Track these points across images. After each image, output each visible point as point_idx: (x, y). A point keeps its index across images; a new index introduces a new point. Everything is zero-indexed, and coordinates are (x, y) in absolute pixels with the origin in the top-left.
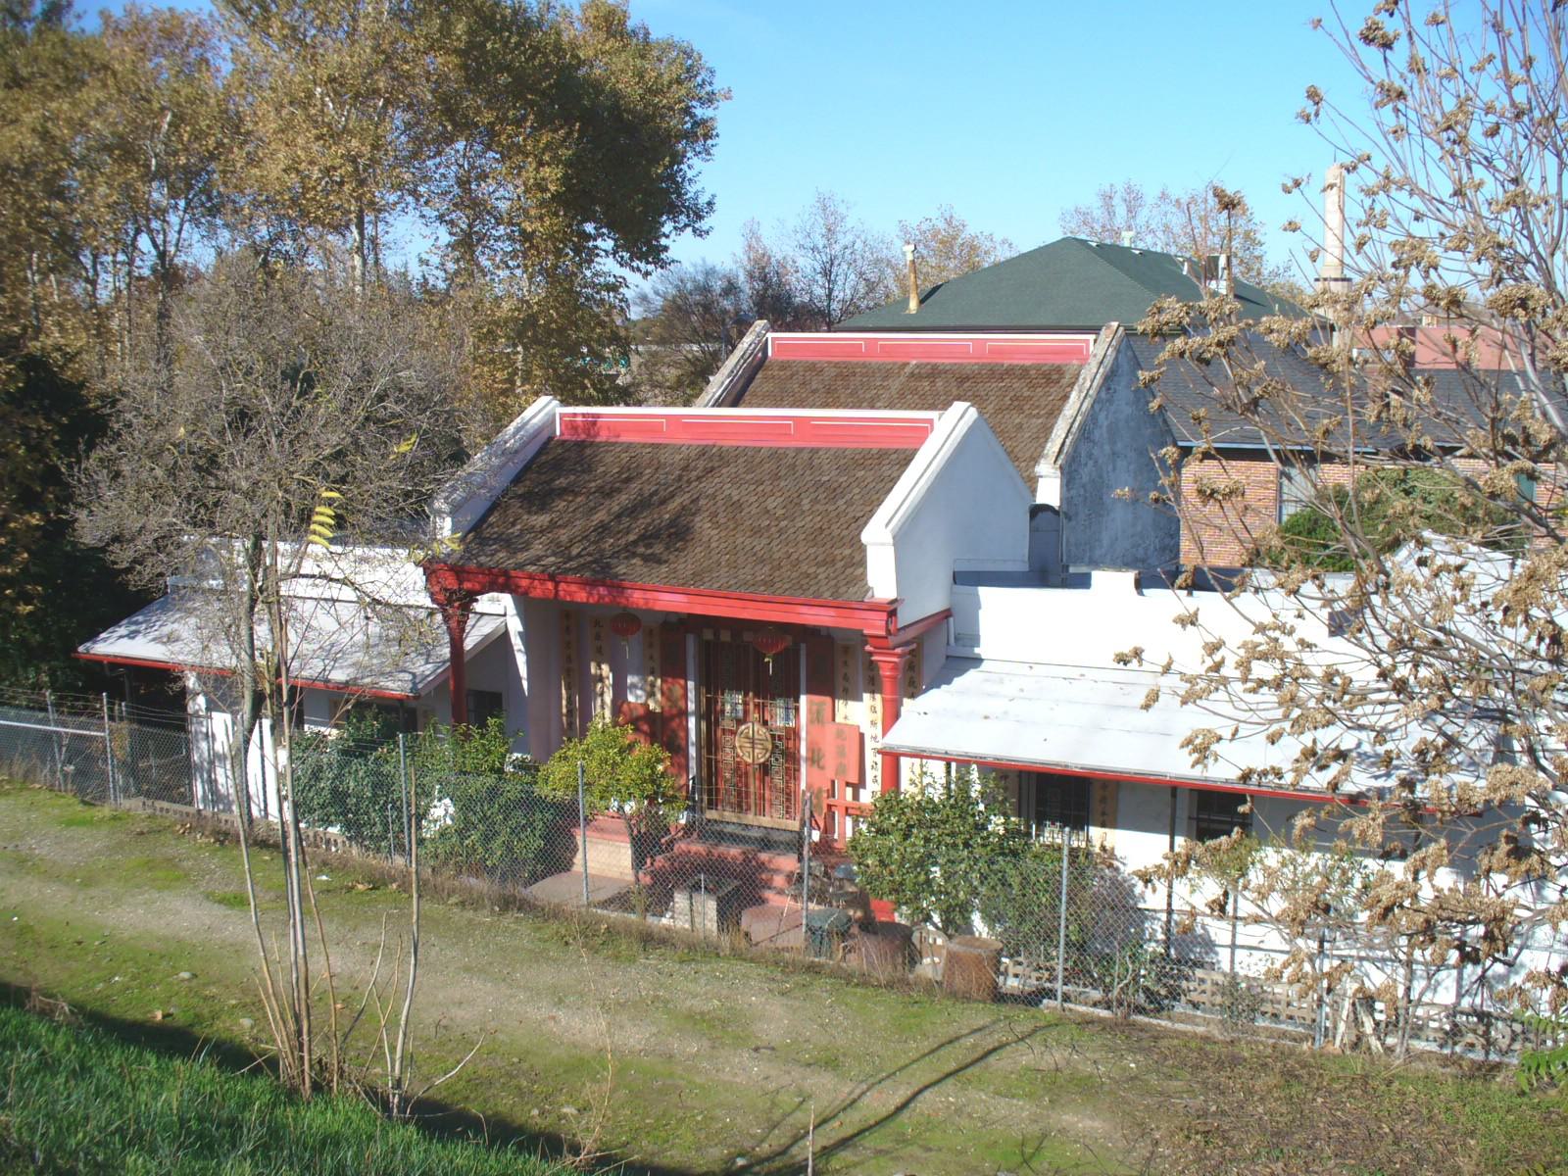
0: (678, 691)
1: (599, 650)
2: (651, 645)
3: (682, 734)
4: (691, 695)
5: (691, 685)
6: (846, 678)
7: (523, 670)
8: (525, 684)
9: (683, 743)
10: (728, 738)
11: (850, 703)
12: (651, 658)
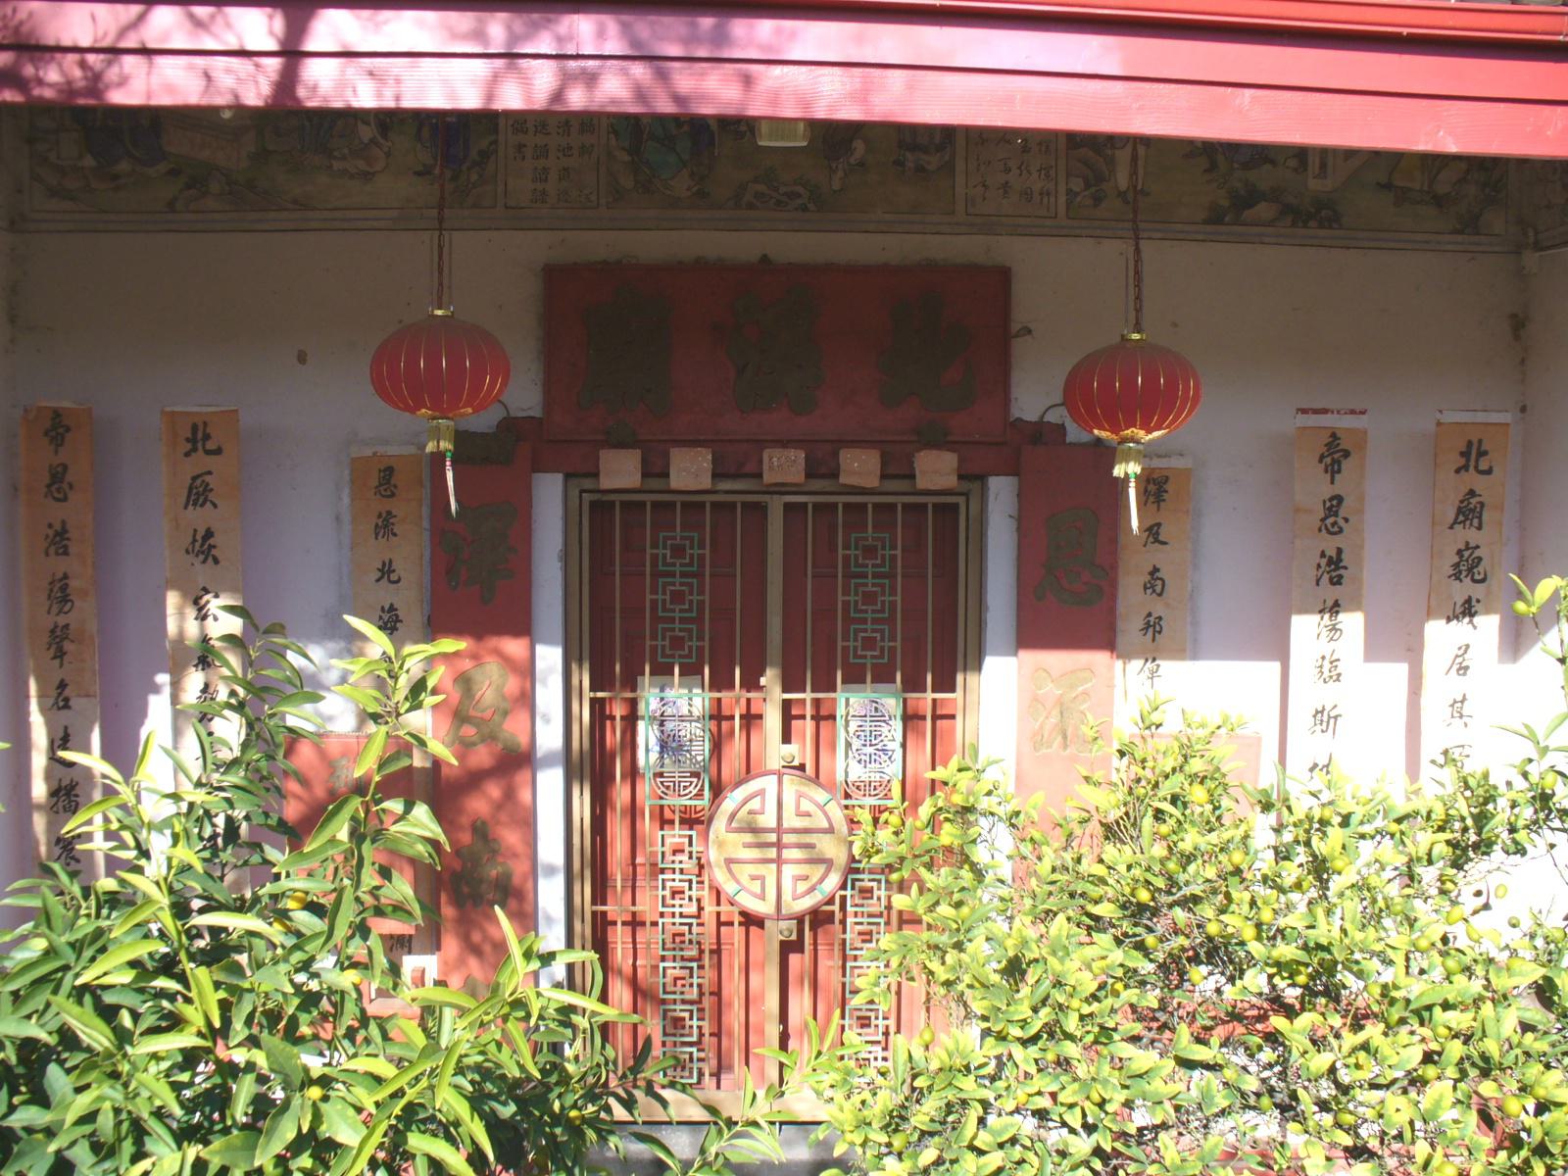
0: (492, 682)
1: (204, 547)
2: (385, 526)
3: (511, 837)
4: (549, 695)
5: (549, 658)
6: (1154, 582)
7: (450, 475)
8: (33, 688)
9: (519, 869)
10: (676, 835)
11: (1168, 667)
12: (386, 571)
